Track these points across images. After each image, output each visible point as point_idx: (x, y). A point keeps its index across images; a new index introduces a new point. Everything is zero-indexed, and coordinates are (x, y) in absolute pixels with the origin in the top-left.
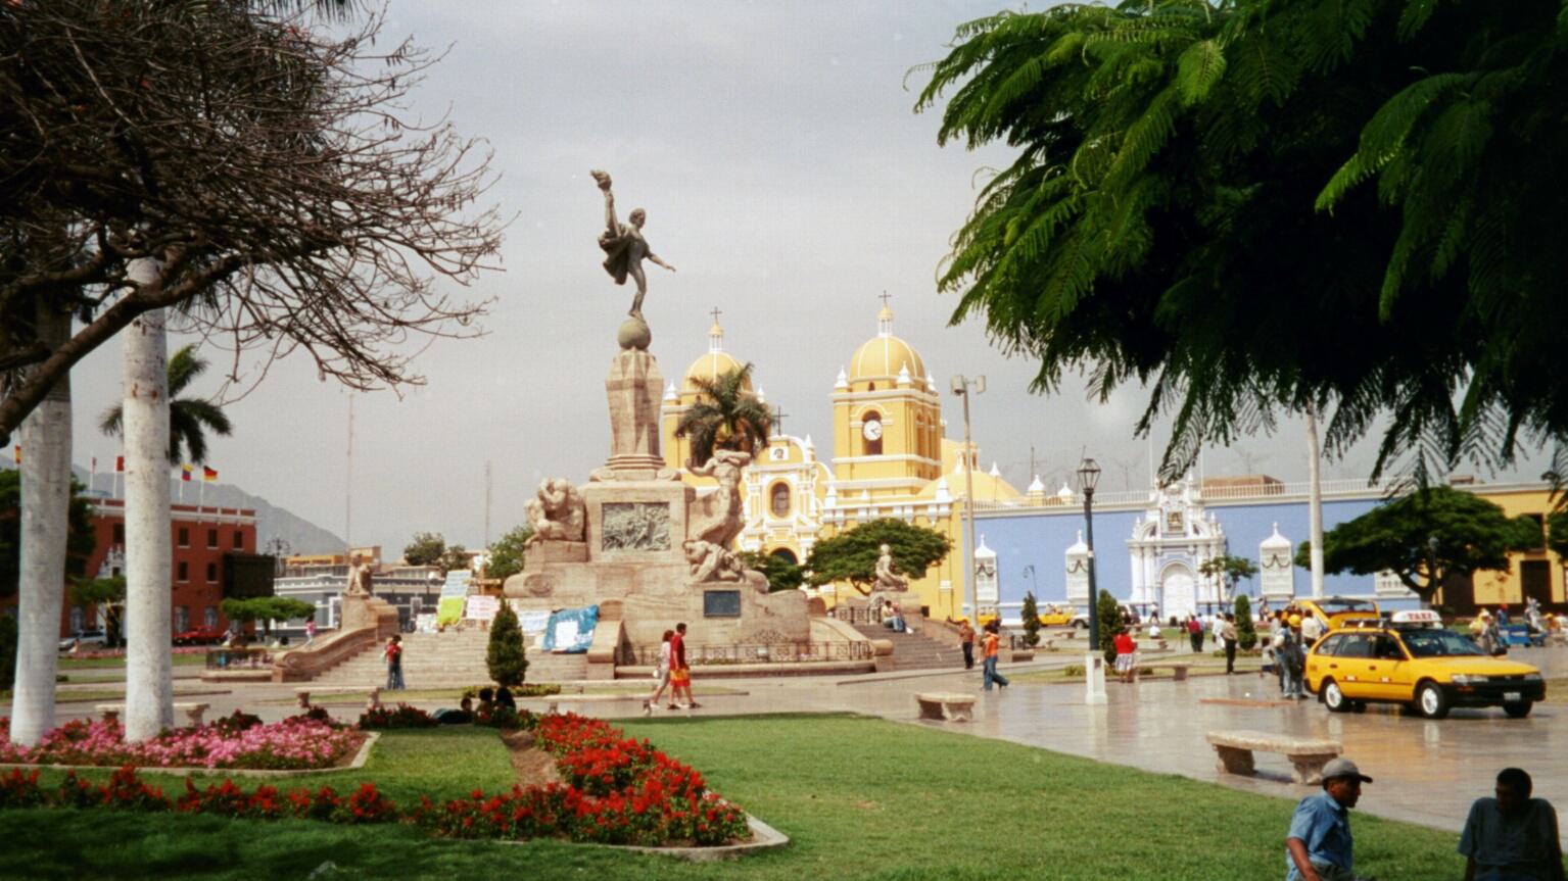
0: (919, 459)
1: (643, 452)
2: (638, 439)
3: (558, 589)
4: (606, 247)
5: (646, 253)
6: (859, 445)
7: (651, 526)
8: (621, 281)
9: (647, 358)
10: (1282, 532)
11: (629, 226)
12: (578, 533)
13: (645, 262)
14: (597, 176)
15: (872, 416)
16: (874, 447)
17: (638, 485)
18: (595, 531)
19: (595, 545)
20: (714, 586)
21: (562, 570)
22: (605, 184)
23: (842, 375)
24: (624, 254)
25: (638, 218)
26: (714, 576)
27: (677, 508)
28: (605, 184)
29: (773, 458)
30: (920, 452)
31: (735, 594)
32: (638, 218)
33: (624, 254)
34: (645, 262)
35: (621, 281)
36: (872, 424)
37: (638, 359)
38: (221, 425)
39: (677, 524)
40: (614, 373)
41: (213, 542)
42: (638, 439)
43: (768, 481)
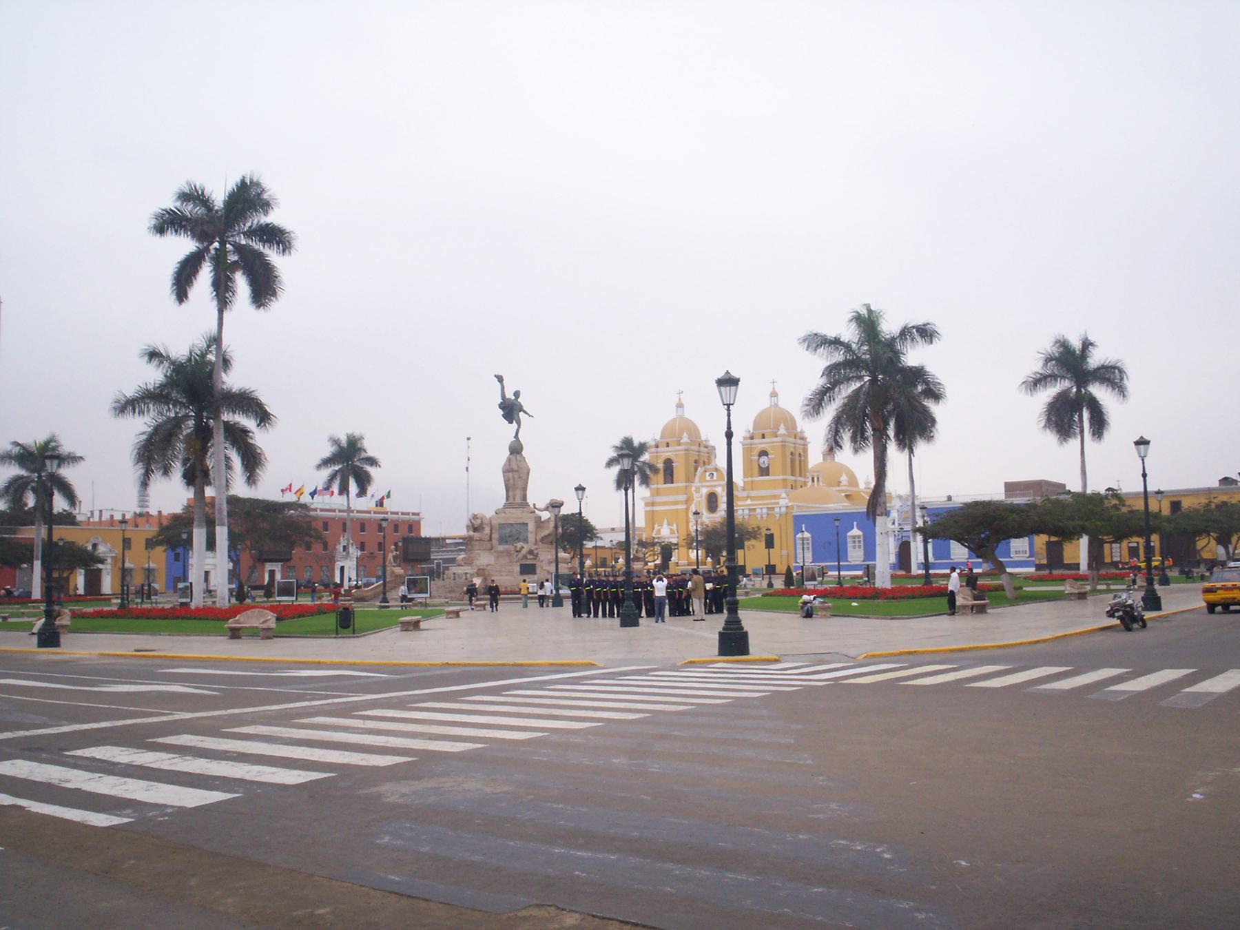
5: (521, 409)
6: (756, 470)
10: (859, 528)
13: (521, 414)
15: (764, 453)
16: (765, 471)
18: (495, 536)
19: (495, 542)
24: (511, 410)
25: (517, 394)
27: (531, 526)
32: (517, 394)
33: (511, 410)
34: (521, 414)
36: (764, 459)
41: (396, 531)
43: (705, 491)
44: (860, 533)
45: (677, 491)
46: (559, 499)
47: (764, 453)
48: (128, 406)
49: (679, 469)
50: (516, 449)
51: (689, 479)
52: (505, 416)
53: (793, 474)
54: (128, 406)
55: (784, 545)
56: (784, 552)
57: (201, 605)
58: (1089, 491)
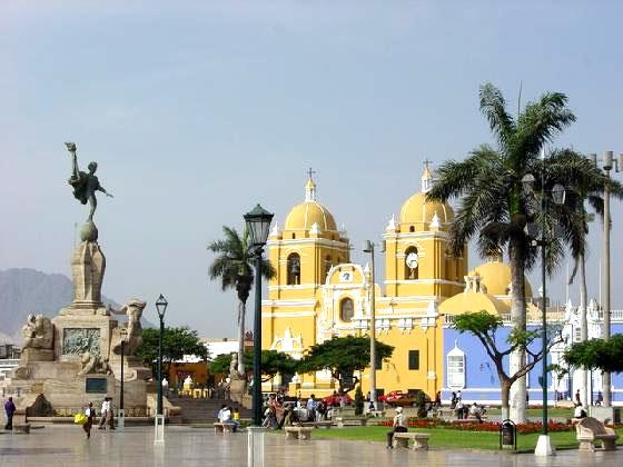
0: (445, 282)
1: (89, 299)
2: (86, 293)
3: (36, 376)
4: (73, 185)
5: (97, 186)
7: (90, 341)
8: (84, 202)
9: (94, 247)
11: (88, 172)
12: (49, 345)
13: (97, 193)
14: (68, 145)
15: (412, 250)
17: (84, 318)
20: (90, 376)
21: (36, 365)
22: (73, 149)
23: (392, 222)
24: (85, 186)
25: (93, 167)
26: (93, 371)
27: (104, 331)
28: (73, 149)
29: (343, 279)
30: (447, 277)
31: (104, 379)
32: (93, 167)
33: (85, 186)
34: (97, 193)
35: (84, 202)
36: (412, 256)
37: (88, 248)
38: (551, 113)
39: (105, 340)
40: (75, 255)
42: (86, 293)
43: (338, 296)
44: (461, 354)
45: (303, 294)
46: (141, 300)
47: (412, 250)
48: (214, 248)
49: (308, 266)
50: (92, 236)
51: (322, 278)
52: (77, 195)
53: (447, 279)
54: (214, 248)
55: (431, 366)
56: (431, 374)
57: (306, 375)
58: (590, 339)
